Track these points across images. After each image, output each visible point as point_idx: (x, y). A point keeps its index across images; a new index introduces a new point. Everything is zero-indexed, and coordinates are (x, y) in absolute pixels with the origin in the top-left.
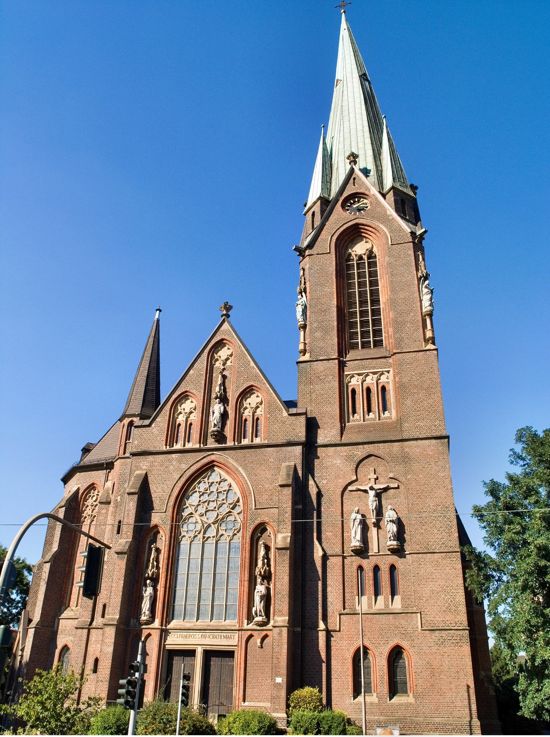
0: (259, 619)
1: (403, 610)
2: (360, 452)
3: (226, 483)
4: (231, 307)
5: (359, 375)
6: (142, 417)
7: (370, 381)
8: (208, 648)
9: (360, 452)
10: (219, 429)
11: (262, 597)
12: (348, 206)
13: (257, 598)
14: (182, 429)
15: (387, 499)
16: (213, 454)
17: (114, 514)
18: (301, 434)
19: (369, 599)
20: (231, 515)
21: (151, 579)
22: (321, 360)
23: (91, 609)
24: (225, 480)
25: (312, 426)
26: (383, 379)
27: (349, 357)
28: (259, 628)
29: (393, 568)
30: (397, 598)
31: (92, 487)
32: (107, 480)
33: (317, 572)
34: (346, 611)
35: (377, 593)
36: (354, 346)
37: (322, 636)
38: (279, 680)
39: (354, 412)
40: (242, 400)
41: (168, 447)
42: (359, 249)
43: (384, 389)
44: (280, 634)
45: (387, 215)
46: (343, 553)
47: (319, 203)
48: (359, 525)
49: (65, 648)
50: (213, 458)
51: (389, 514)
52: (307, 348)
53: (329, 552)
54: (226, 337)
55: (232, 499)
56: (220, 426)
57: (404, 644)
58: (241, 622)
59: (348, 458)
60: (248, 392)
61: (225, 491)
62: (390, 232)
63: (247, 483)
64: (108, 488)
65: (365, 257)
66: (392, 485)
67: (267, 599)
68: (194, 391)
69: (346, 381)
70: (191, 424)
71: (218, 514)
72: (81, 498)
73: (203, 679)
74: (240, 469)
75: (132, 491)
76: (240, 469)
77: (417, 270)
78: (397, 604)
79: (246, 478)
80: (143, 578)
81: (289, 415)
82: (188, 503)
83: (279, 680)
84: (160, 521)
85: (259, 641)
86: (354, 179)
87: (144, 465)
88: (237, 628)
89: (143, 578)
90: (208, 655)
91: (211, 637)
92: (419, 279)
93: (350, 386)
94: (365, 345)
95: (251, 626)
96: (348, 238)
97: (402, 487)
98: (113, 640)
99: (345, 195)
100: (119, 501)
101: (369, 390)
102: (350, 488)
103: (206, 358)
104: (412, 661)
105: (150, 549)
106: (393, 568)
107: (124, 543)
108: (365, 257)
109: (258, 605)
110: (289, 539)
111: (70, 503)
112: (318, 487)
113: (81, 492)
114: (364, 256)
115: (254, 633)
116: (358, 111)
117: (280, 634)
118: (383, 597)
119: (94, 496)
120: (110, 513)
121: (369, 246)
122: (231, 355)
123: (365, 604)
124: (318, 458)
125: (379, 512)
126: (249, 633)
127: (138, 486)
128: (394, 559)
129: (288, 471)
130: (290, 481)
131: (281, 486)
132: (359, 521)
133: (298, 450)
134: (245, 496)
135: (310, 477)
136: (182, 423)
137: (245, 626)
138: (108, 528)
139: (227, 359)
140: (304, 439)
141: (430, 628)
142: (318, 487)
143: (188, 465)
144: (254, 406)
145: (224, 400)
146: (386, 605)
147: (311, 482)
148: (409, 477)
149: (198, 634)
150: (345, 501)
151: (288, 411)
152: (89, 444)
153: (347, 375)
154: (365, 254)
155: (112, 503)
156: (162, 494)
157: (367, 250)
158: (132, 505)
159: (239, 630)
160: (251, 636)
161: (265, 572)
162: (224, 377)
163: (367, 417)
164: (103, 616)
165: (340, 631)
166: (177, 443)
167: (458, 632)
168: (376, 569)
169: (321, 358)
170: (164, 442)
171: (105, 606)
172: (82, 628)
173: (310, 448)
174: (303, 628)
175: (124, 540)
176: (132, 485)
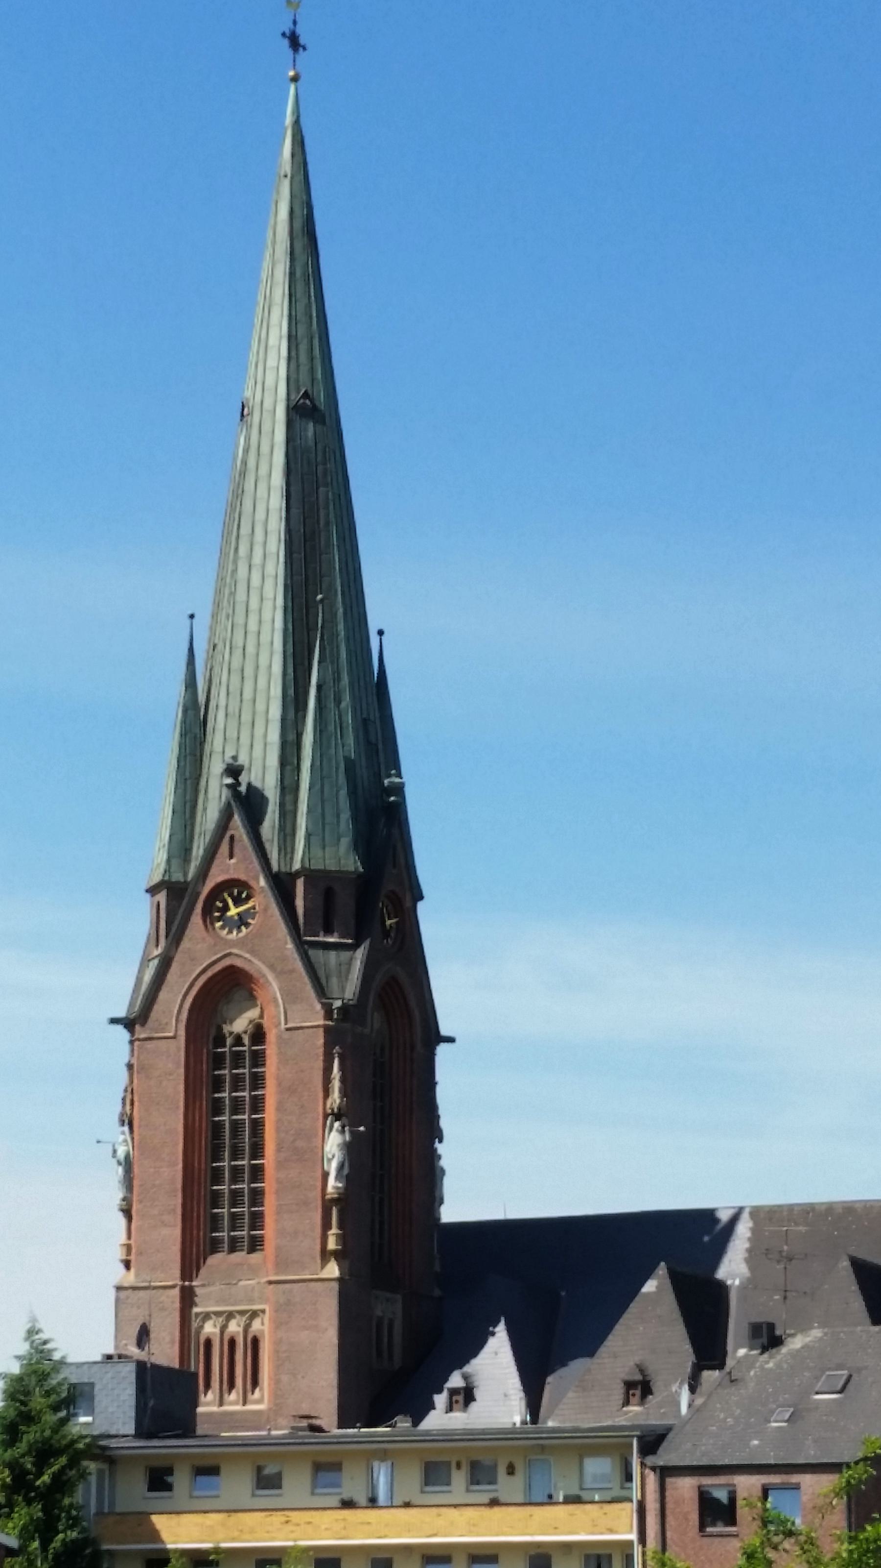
7: (235, 1327)
22: (155, 1288)
26: (256, 1325)
33: (343, 1080)
36: (214, 1247)
39: (208, 1386)
43: (256, 1342)
52: (132, 1257)
65: (246, 1040)
69: (194, 1325)
99: (210, 884)
101: (232, 1343)
108: (246, 1040)
114: (243, 1036)
116: (270, 569)
124: (18, 1358)
135: (678, 1384)
153: (197, 1315)
154: (245, 1032)
165: (191, 1497)
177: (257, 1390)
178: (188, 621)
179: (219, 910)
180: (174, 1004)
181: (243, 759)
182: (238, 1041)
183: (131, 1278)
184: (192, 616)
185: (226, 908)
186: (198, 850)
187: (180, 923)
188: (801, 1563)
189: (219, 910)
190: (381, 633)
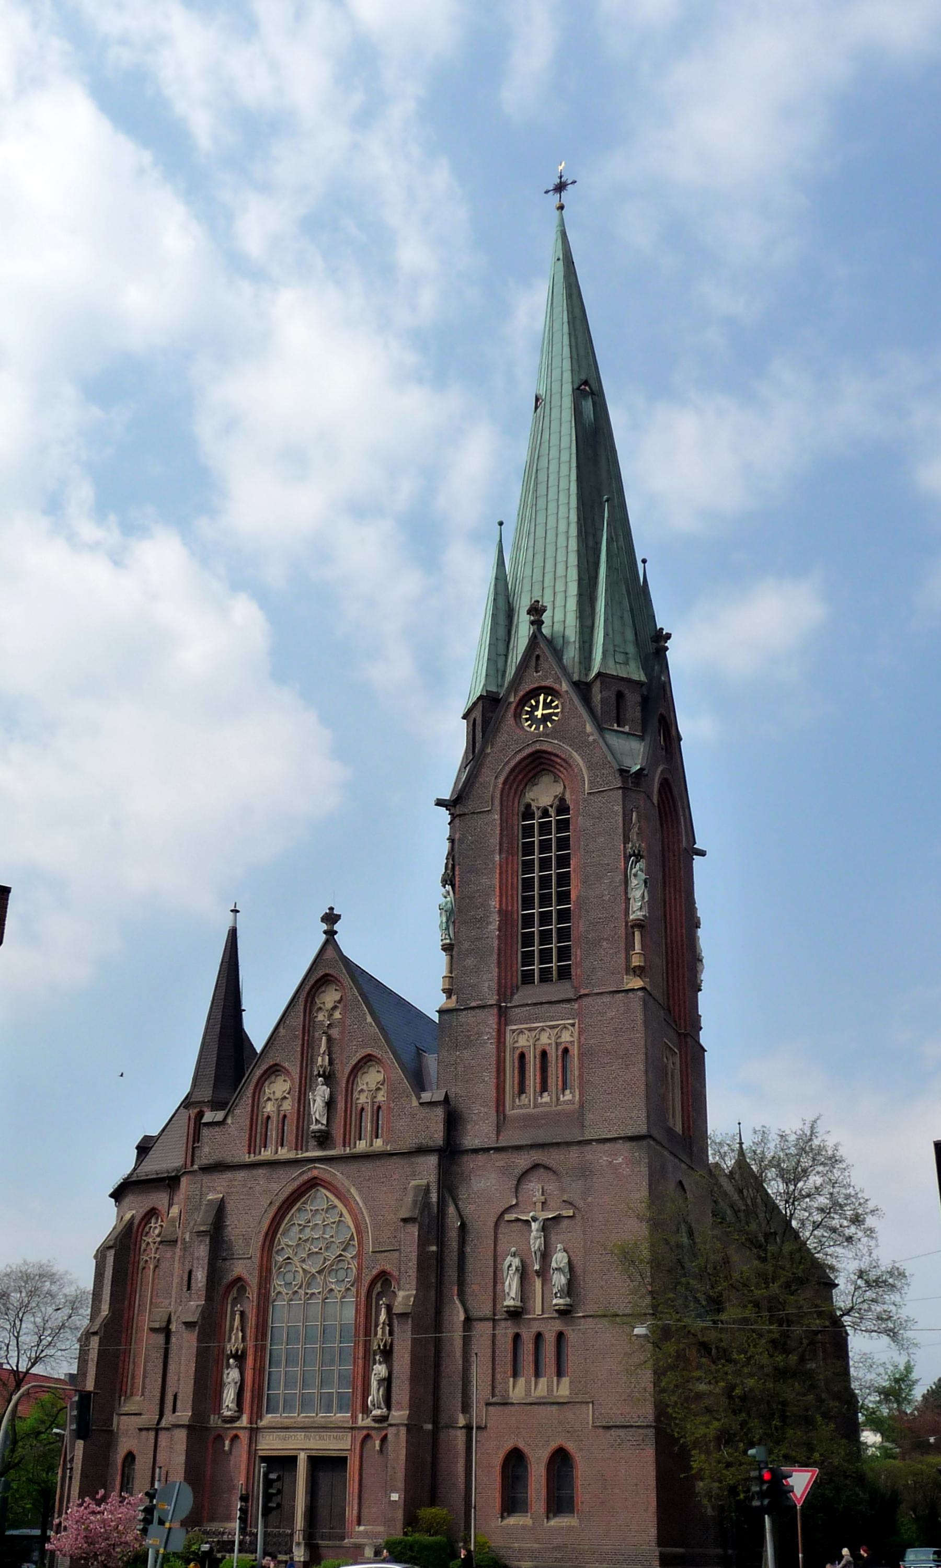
0: (377, 1412)
1: (572, 1398)
2: (523, 1161)
3: (336, 1211)
4: (338, 917)
5: (530, 1030)
6: (216, 1105)
7: (544, 1039)
8: (314, 1453)
9: (523, 1161)
10: (323, 1127)
11: (380, 1382)
12: (527, 713)
13: (374, 1384)
14: (273, 1125)
15: (557, 1234)
16: (315, 1168)
17: (183, 1258)
18: (437, 1135)
19: (528, 1382)
20: (343, 1260)
21: (235, 1356)
22: (473, 1008)
23: (158, 1402)
24: (336, 1206)
25: (453, 1121)
27: (517, 999)
28: (377, 1425)
29: (560, 1336)
30: (565, 1380)
31: (152, 1213)
32: (170, 1205)
34: (494, 1400)
35: (537, 1375)
37: (461, 1435)
38: (395, 1497)
40: (356, 1076)
41: (252, 1155)
42: (543, 795)
44: (397, 1434)
45: (585, 733)
46: (494, 1314)
47: (480, 703)
48: (514, 1274)
49: (130, 1457)
50: (315, 1173)
51: (559, 1259)
53: (475, 1314)
54: (331, 972)
55: (344, 1236)
56: (325, 1122)
57: (570, 1446)
58: (354, 1418)
59: (504, 1171)
60: (367, 1060)
61: (334, 1223)
62: (589, 769)
63: (362, 1213)
64: (173, 1217)
65: (552, 812)
66: (565, 1213)
67: (387, 1382)
68: (286, 1065)
70: (285, 1116)
71: (325, 1259)
72: (137, 1231)
73: (309, 1496)
74: (353, 1190)
75: (202, 1228)
76: (353, 1190)
77: (626, 839)
78: (564, 1390)
79: (361, 1205)
80: (225, 1356)
81: (421, 1104)
82: (285, 1241)
83: (395, 1497)
84: (245, 1272)
85: (378, 1443)
86: (538, 657)
87: (215, 1189)
88: (350, 1425)
89: (225, 1356)
90: (318, 1463)
91: (317, 1438)
92: (627, 858)
93: (518, 1048)
94: (545, 976)
95: (368, 1422)
96: (525, 776)
97: (578, 1216)
98: (185, 1446)
100: (187, 1240)
101: (544, 1054)
102: (507, 1217)
103: (302, 1007)
104: (582, 1471)
105: (233, 1314)
106: (560, 1336)
107: (194, 1307)
108: (552, 812)
109: (376, 1393)
110: (412, 1299)
111: (121, 1242)
112: (461, 1217)
113: (136, 1222)
115: (373, 1433)
116: (563, 484)
117: (397, 1434)
118: (546, 1379)
119: (156, 1227)
120: (177, 1258)
121: (558, 789)
122: (339, 1002)
123: (518, 1391)
125: (545, 1256)
126: (365, 1432)
127: (210, 1220)
128: (558, 1326)
129: (416, 1196)
130: (416, 1214)
131: (405, 1220)
132: (514, 1268)
133: (433, 1160)
134: (359, 1232)
135: (451, 1202)
136: (272, 1115)
137: (360, 1423)
138: (176, 1280)
139: (334, 1008)
140: (441, 1143)
141: (604, 1424)
142: (461, 1217)
143: (284, 1184)
144: (373, 1087)
145: (329, 1078)
146: (550, 1390)
147: (451, 1209)
148: (590, 1199)
149: (301, 1435)
150: (500, 1236)
151: (419, 1098)
152: (146, 1138)
154: (551, 806)
155: (179, 1243)
156: (245, 1228)
157: (556, 797)
158: (202, 1250)
159: (352, 1428)
160: (367, 1436)
161: (385, 1345)
162: (330, 1040)
163: (539, 1101)
164: (174, 1412)
166: (265, 1147)
167: (641, 1431)
168: (539, 1337)
169: (473, 1004)
170: (246, 1148)
171: (175, 1396)
172: (148, 1429)
173: (450, 1152)
174: (435, 1423)
175: (193, 1306)
176: (202, 1220)
177: (567, 1092)
178: (557, 213)
179: (531, 706)
180: (493, 781)
181: (547, 601)
182: (545, 813)
183: (452, 1004)
184: (501, 524)
185: (536, 708)
186: (511, 671)
187: (294, 1499)
188: (908, 1285)
189: (531, 706)
190: (644, 561)
